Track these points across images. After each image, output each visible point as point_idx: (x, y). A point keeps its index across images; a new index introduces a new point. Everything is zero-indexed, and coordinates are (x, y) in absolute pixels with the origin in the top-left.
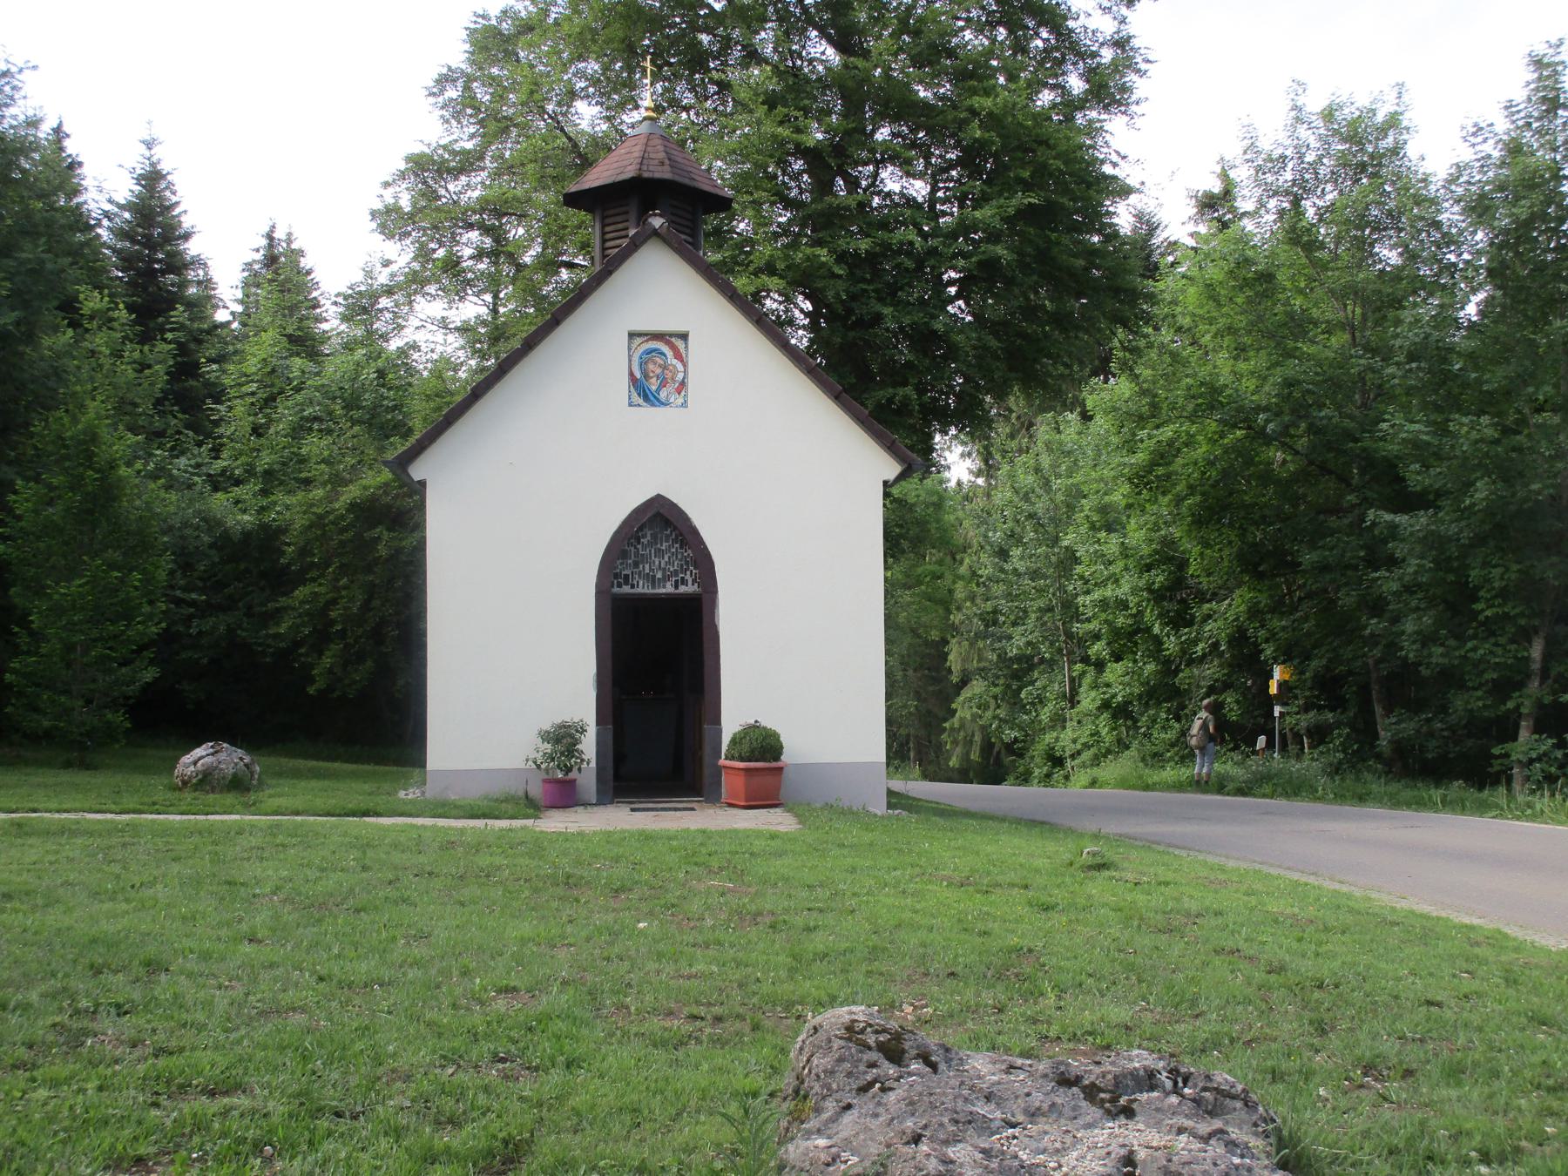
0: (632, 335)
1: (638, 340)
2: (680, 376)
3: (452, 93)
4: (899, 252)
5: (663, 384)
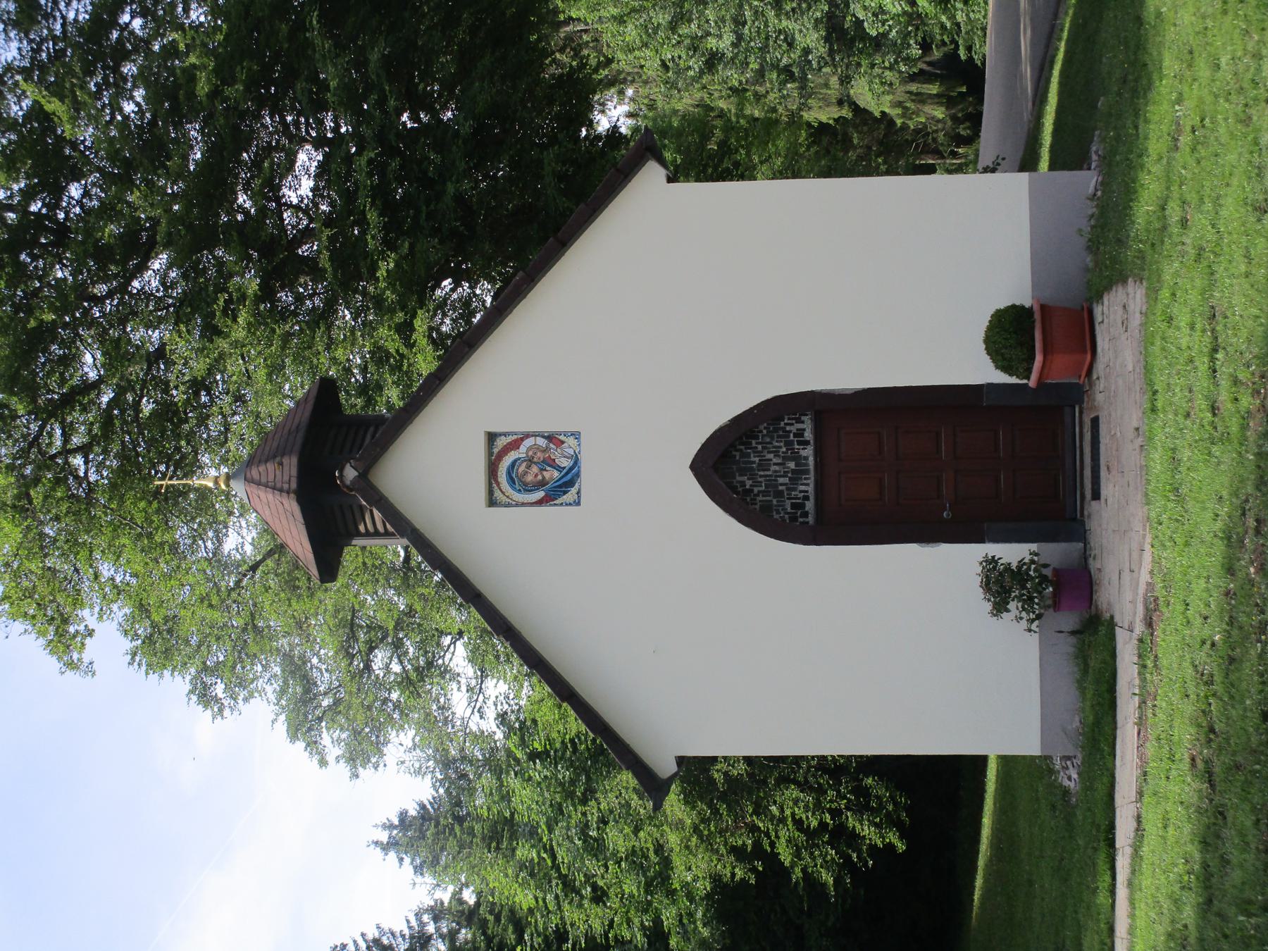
0: (492, 503)
1: (497, 493)
2: (542, 442)
3: (219, 689)
4: (383, 175)
5: (552, 463)
